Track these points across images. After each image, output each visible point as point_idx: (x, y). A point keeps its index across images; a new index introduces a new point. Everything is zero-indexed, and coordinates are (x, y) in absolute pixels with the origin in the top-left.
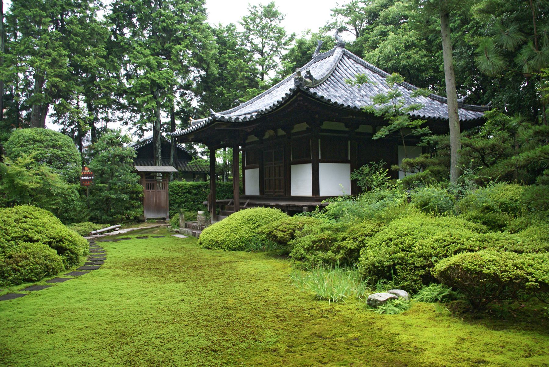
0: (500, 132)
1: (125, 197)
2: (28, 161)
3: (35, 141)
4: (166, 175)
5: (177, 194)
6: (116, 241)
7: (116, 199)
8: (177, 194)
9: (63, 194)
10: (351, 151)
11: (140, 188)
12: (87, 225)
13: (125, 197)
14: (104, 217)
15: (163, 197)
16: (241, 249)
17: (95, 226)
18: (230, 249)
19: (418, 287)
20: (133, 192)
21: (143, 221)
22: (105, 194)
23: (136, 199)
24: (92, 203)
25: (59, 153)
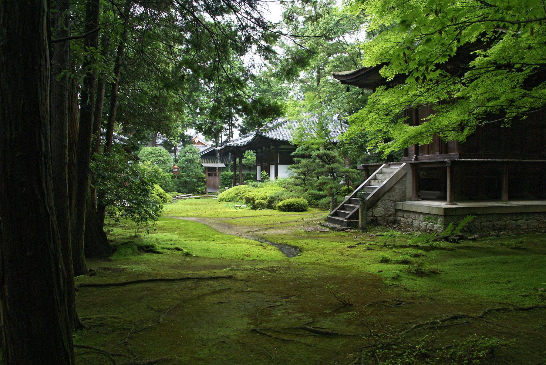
0: (168, 356)
1: (194, 180)
2: (149, 164)
3: (152, 154)
4: (220, 168)
5: (225, 179)
6: (186, 199)
7: (190, 181)
8: (225, 179)
9: (164, 178)
10: (451, 182)
11: (204, 175)
12: (175, 193)
13: (194, 180)
14: (184, 190)
15: (217, 180)
16: (230, 201)
17: (178, 194)
18: (226, 201)
19: (393, 328)
20: (200, 178)
21: (205, 193)
22: (185, 178)
23: (202, 182)
24: (178, 183)
25: (162, 159)
